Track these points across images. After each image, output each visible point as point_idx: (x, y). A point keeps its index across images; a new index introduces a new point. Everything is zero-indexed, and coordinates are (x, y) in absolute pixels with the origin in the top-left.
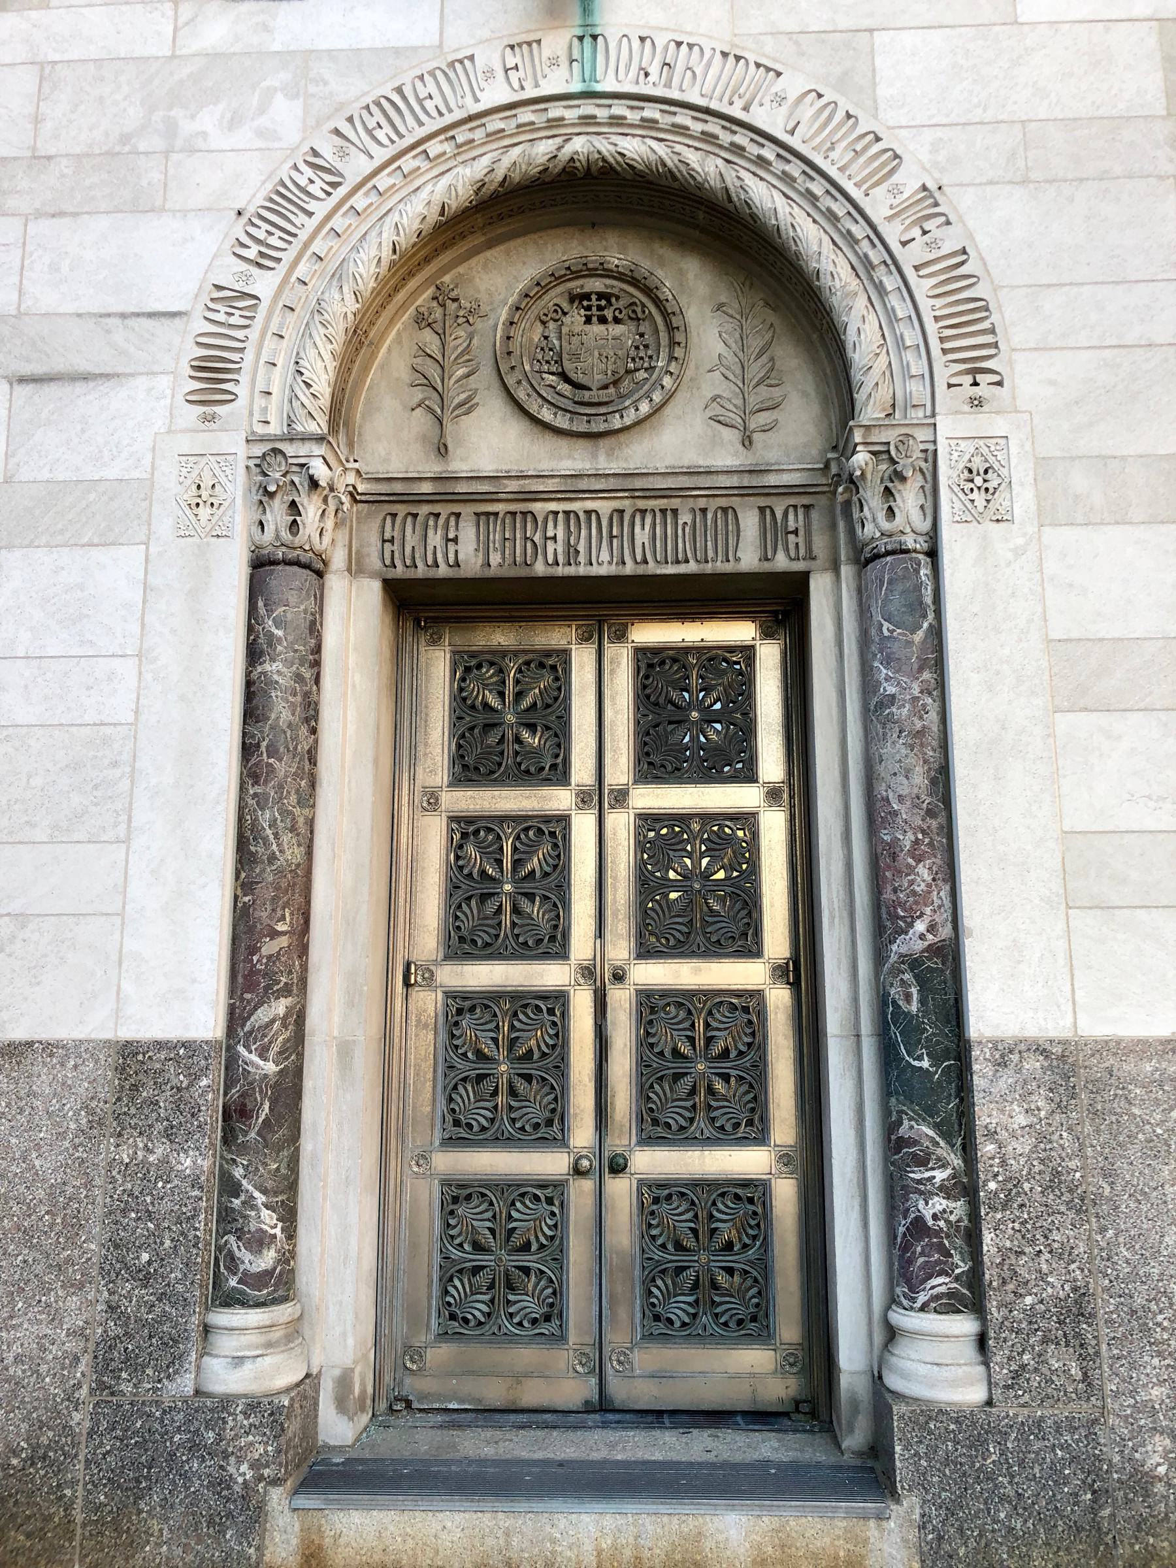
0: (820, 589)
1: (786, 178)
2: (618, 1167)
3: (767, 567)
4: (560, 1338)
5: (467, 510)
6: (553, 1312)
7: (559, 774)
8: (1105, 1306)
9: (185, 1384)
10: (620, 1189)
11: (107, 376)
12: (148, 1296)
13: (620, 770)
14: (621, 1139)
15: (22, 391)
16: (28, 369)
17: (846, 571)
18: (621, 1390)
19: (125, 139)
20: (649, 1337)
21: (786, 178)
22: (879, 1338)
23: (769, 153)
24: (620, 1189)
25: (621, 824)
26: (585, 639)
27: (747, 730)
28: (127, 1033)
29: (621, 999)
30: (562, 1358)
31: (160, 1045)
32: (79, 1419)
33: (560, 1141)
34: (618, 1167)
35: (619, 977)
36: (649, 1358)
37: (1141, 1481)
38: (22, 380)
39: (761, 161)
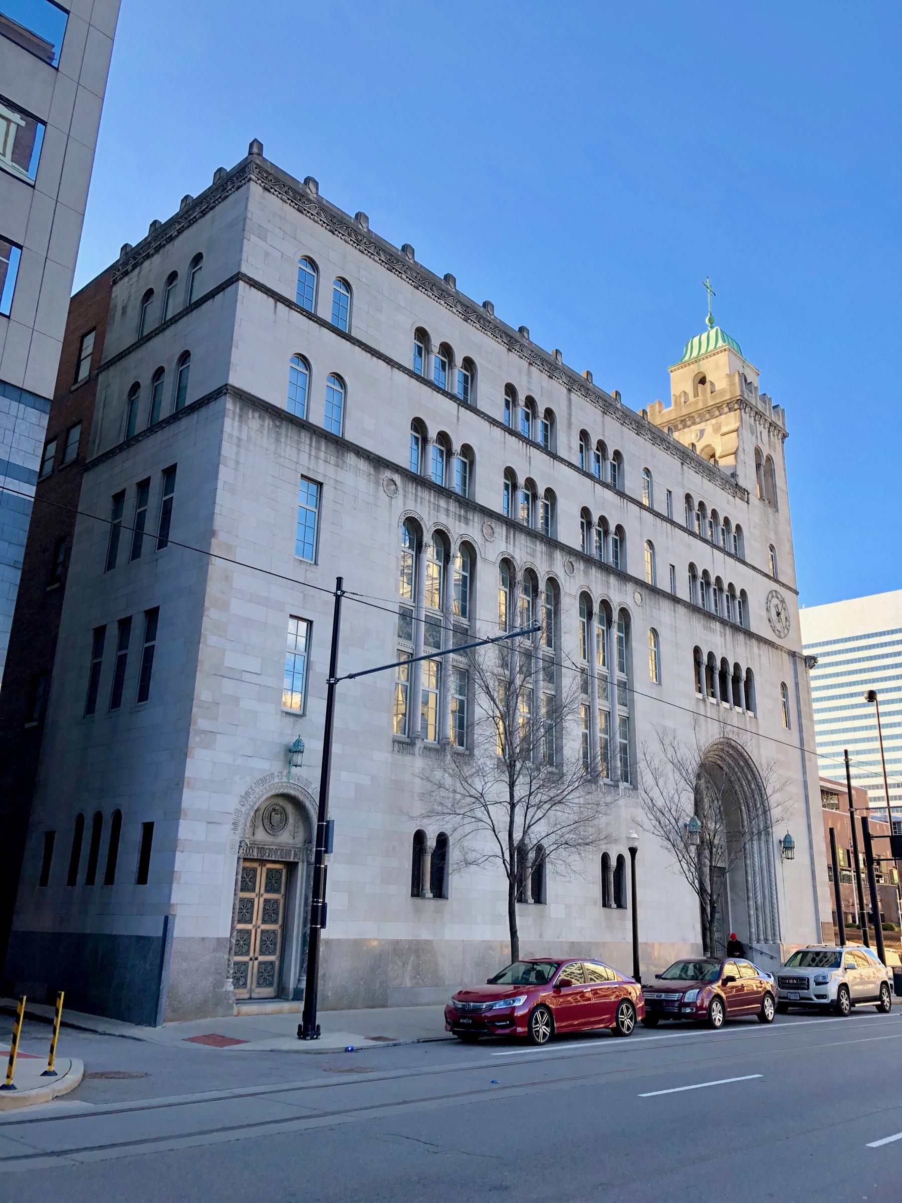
0: (300, 865)
1: (311, 801)
2: (256, 959)
3: (294, 861)
4: (246, 987)
5: (256, 846)
6: (245, 984)
7: (253, 890)
8: (327, 975)
9: (224, 990)
10: (256, 962)
11: (220, 823)
12: (220, 977)
13: (262, 891)
14: (257, 955)
15: (209, 824)
16: (210, 821)
17: (305, 863)
18: (254, 996)
19: (225, 779)
20: (257, 987)
21: (311, 801)
22: (297, 981)
23: (309, 796)
24: (256, 962)
25: (262, 900)
26: (259, 866)
27: (280, 887)
28: (218, 937)
29: (259, 931)
30: (245, 991)
31: (223, 938)
32: (210, 995)
33: (248, 955)
34: (256, 959)
35: (259, 927)
36: (258, 990)
37: (328, 997)
38: (208, 823)
39: (308, 797)
